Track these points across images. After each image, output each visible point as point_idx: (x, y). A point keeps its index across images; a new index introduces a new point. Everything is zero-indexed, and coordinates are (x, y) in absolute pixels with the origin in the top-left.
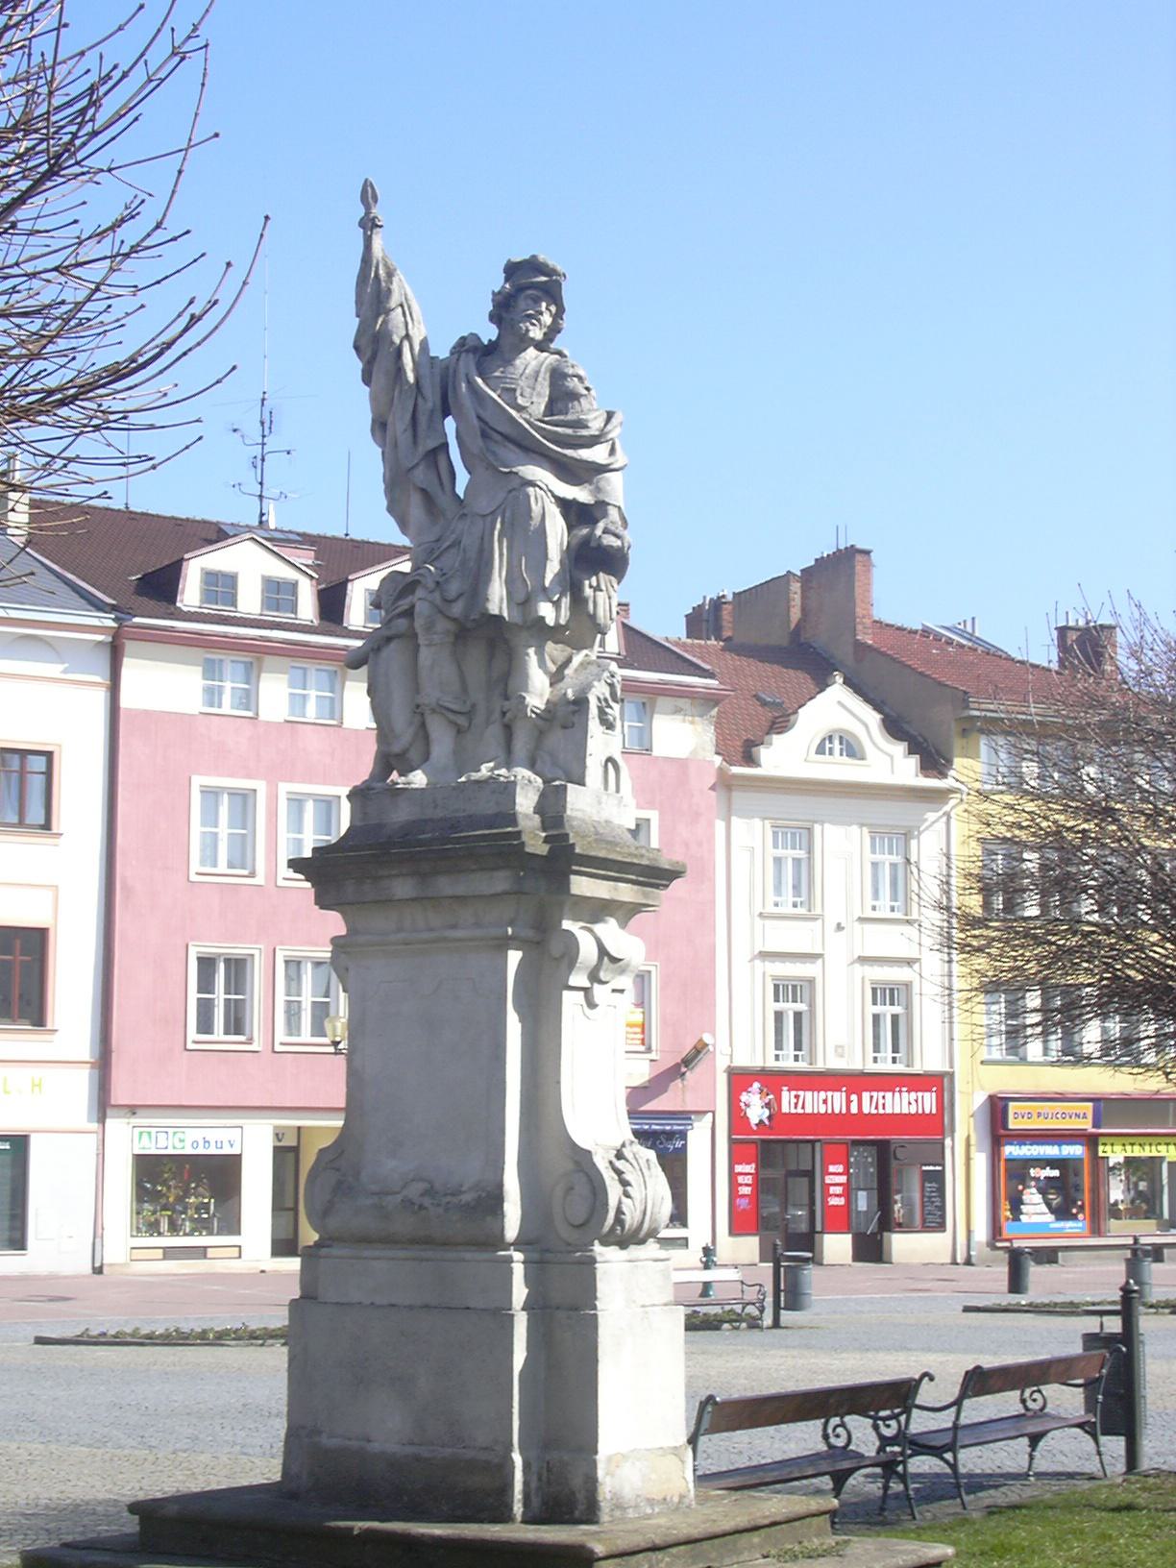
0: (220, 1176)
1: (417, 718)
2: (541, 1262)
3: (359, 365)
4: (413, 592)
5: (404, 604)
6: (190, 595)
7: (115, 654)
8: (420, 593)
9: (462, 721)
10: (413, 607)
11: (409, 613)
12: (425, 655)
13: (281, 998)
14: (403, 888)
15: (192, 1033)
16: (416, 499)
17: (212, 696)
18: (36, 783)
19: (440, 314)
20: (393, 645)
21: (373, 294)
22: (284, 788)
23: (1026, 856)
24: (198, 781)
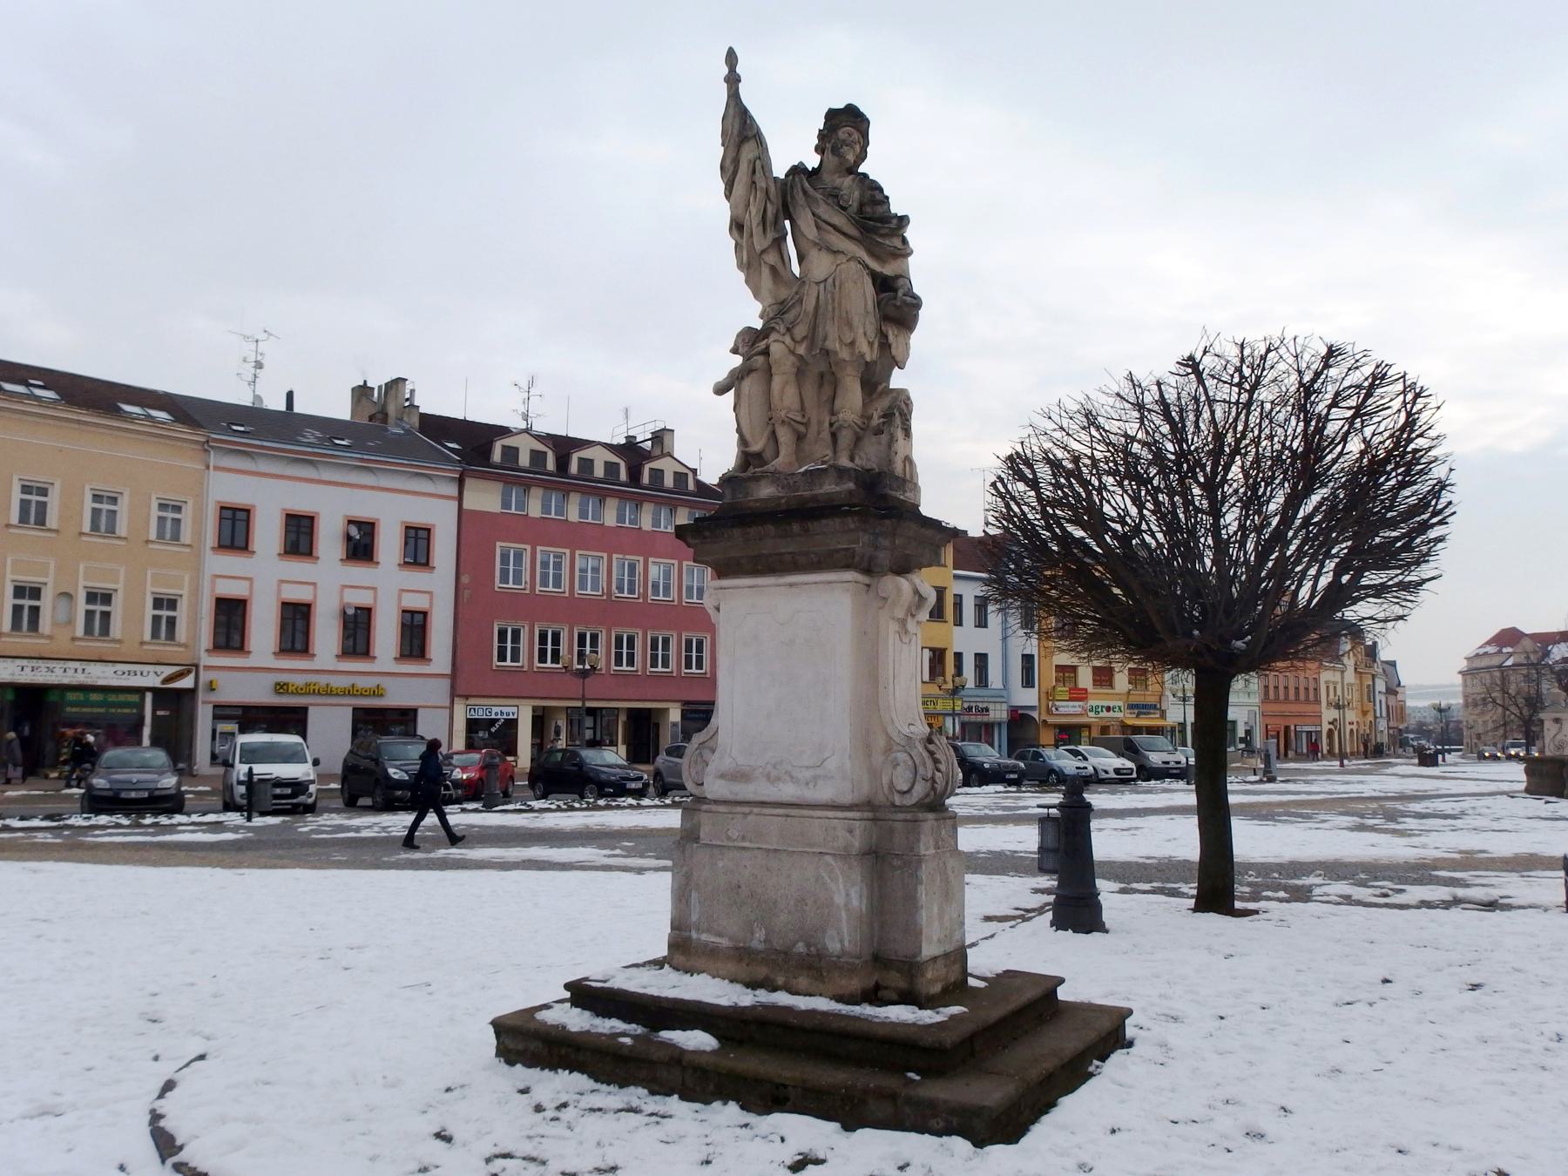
0: (669, 753)
1: (770, 428)
2: (874, 820)
3: (723, 186)
4: (767, 337)
5: (762, 345)
6: (497, 456)
7: (461, 483)
8: (773, 336)
9: (802, 429)
10: (768, 347)
11: (766, 352)
12: (777, 381)
13: (537, 647)
14: (796, 527)
15: (496, 662)
16: (766, 272)
17: (506, 504)
18: (422, 544)
19: (792, 145)
20: (754, 375)
21: (741, 132)
22: (539, 548)
23: (1154, 545)
24: (499, 544)
